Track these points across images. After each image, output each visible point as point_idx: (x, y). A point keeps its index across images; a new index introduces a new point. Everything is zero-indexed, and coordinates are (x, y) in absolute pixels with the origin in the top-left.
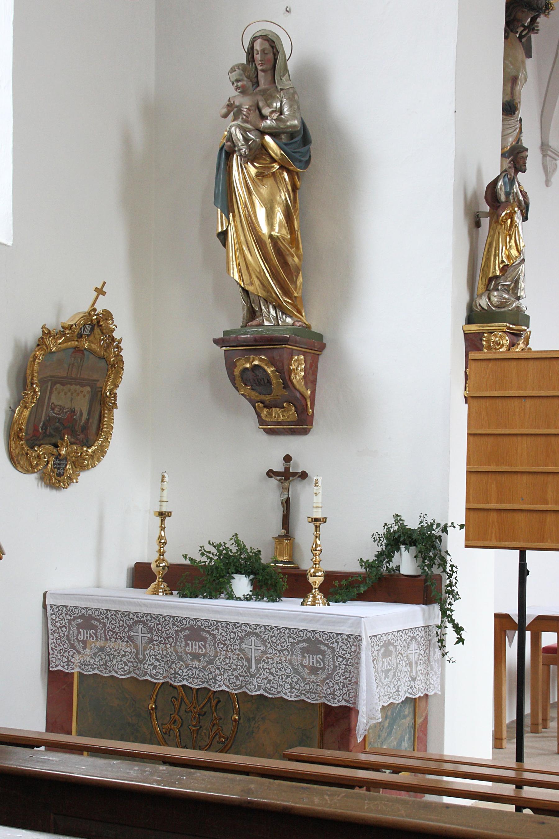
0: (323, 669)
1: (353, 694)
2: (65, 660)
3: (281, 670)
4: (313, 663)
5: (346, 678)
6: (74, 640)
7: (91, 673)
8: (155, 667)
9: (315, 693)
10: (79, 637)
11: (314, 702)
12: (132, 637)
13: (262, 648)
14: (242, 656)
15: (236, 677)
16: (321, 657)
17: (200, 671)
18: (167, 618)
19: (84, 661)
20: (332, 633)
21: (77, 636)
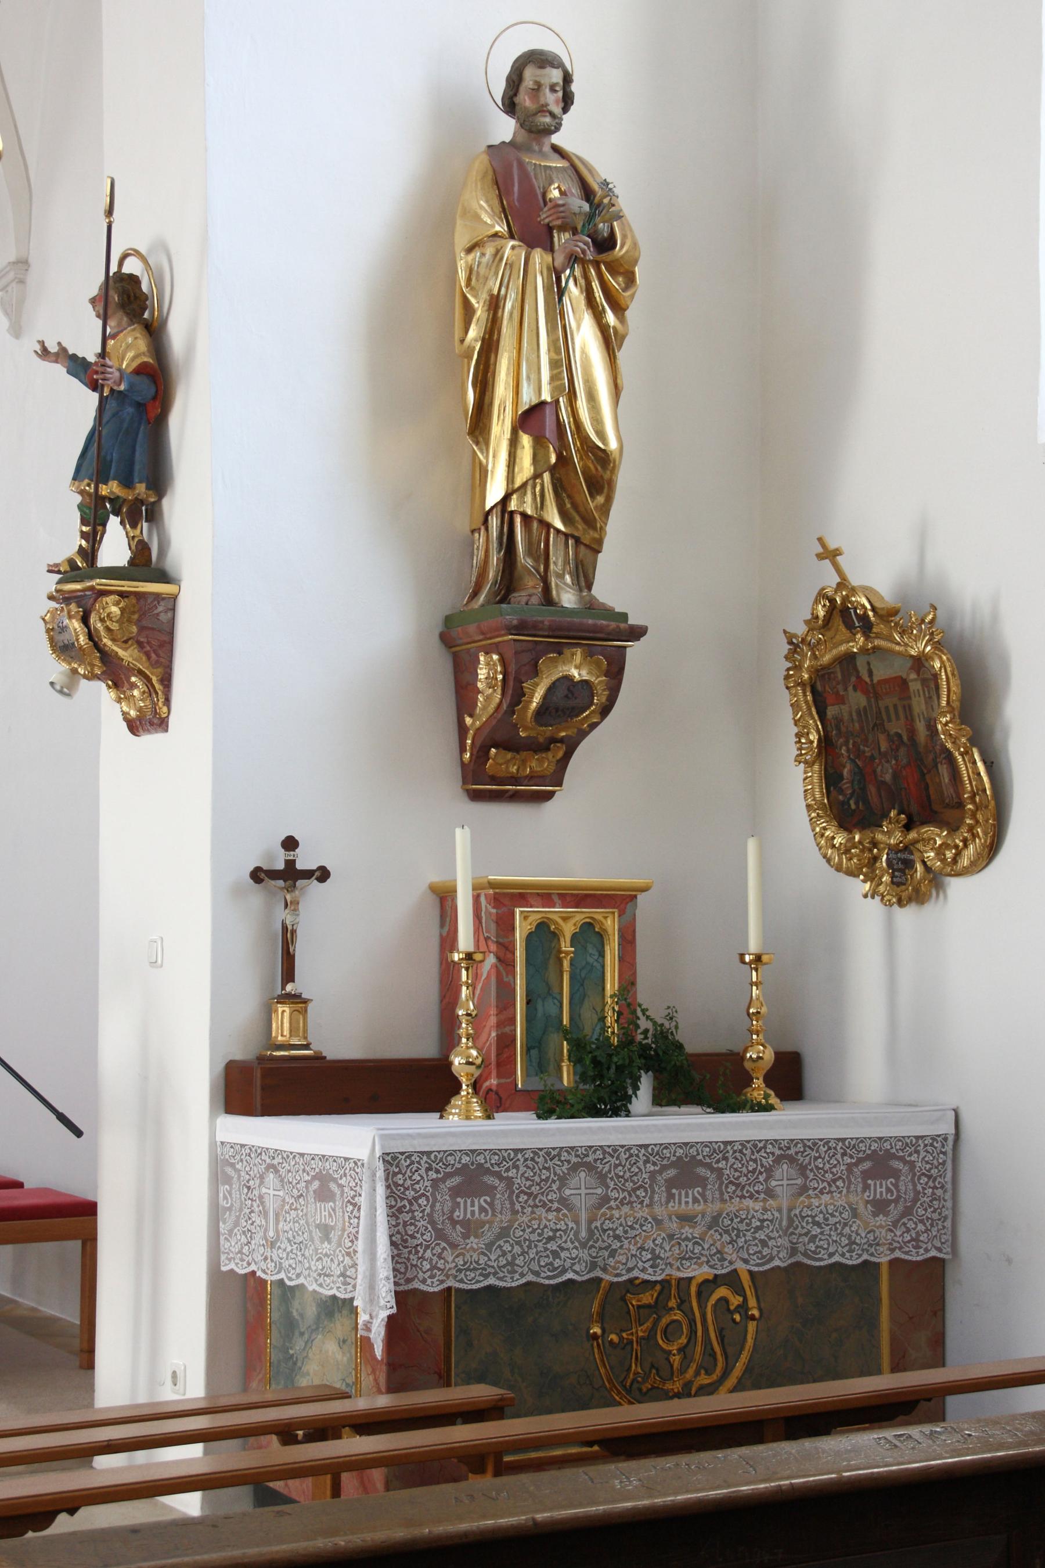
0: (896, 1201)
1: (755, 1248)
2: (845, 1241)
3: (634, 1229)
4: (473, 1212)
5: (934, 1212)
6: (443, 1223)
7: (482, 1285)
8: (813, 1239)
9: (475, 1269)
10: (457, 1213)
11: (474, 1287)
12: (772, 1191)
13: (599, 1191)
14: (565, 1211)
15: (761, 1241)
16: (488, 1199)
17: (694, 1243)
18: (832, 1144)
19: (465, 1263)
20: (506, 1150)
21: (452, 1212)
